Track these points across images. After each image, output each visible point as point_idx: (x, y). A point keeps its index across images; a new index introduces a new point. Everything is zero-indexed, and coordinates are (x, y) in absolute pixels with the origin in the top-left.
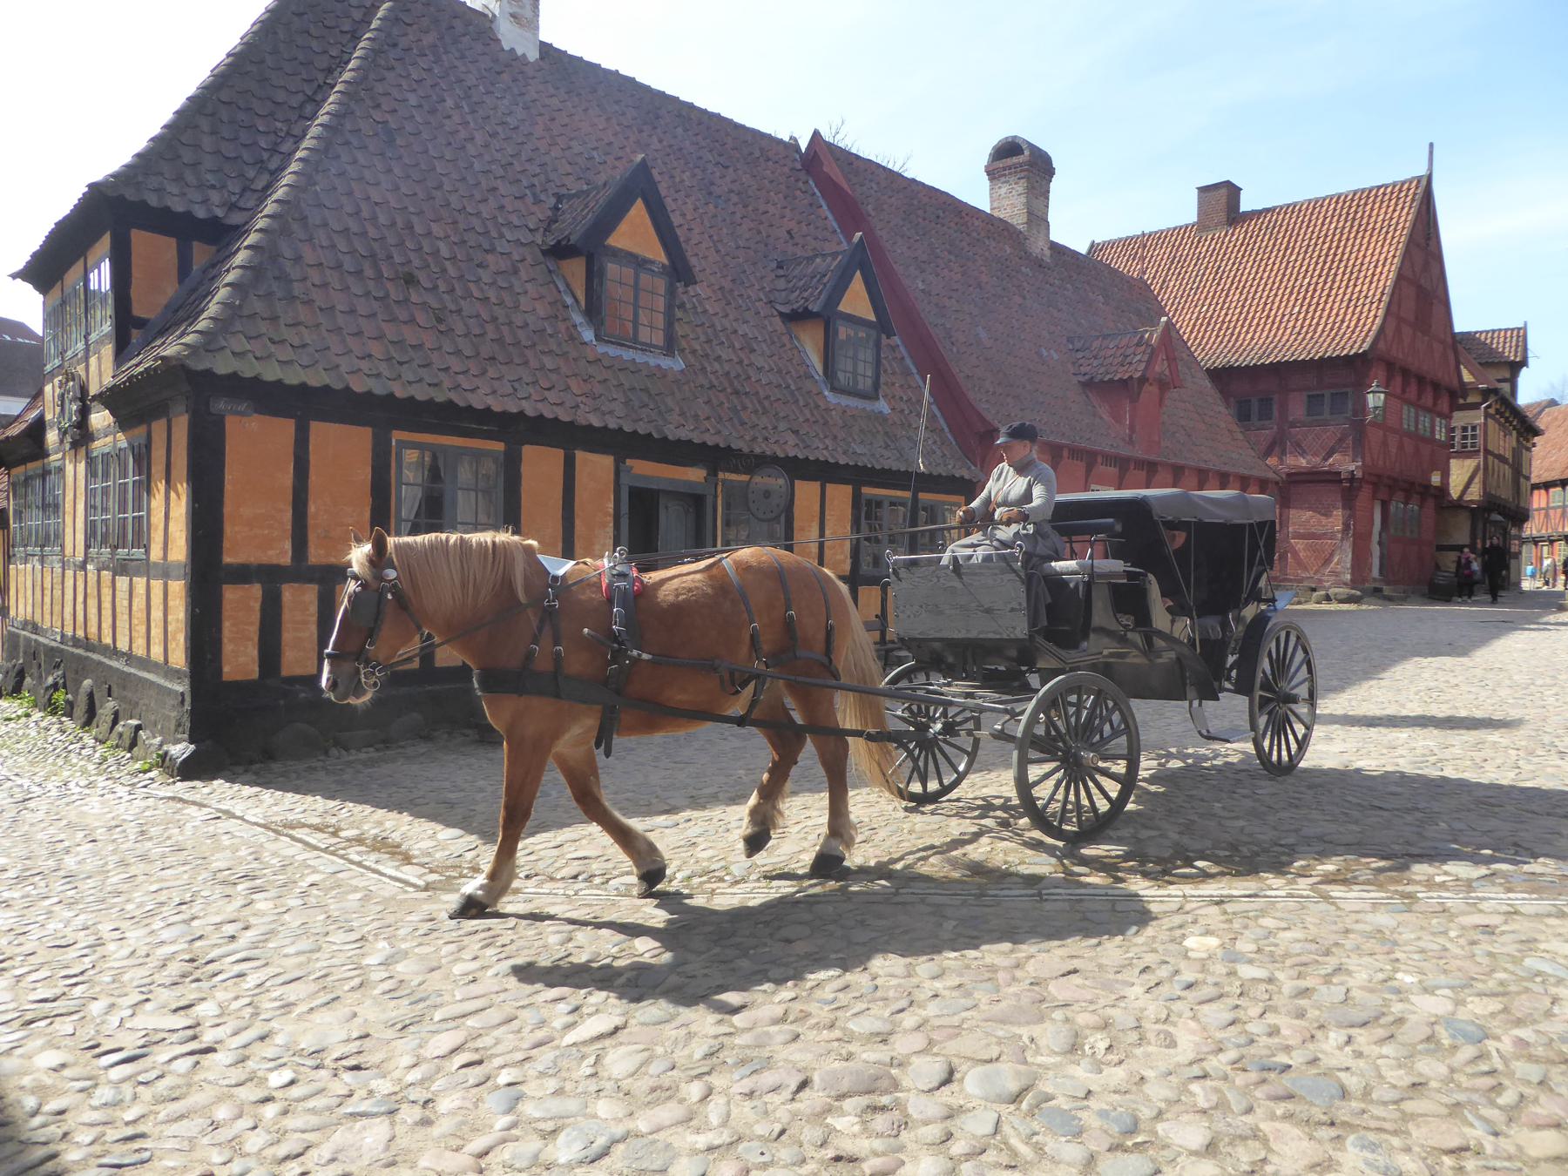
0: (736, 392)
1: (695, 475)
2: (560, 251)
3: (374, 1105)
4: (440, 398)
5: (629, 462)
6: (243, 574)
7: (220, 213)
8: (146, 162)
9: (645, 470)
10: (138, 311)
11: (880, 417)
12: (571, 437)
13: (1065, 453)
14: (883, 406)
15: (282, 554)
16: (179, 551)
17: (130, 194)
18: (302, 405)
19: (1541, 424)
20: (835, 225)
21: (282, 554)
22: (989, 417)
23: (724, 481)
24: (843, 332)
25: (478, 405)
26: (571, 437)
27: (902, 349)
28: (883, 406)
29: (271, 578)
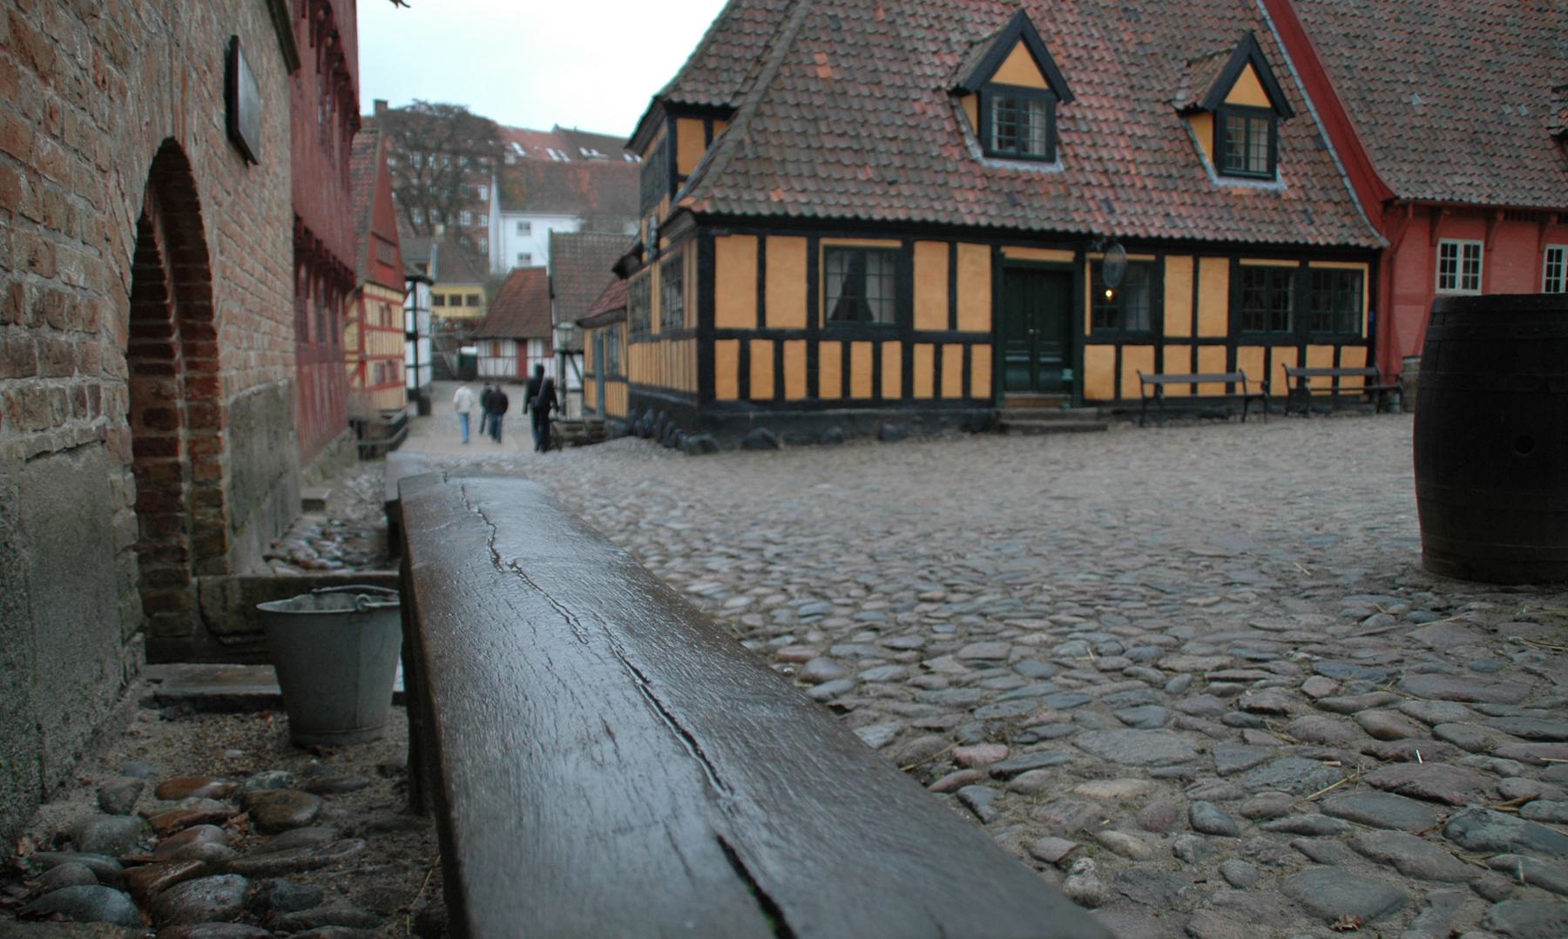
0: (1112, 186)
1: (1064, 256)
2: (959, 92)
3: (248, 100)
4: (849, 214)
5: (1003, 249)
6: (728, 334)
7: (728, 100)
8: (698, 64)
9: (1013, 253)
10: (682, 171)
11: (1277, 195)
12: (952, 234)
13: (1500, 217)
14: (1281, 184)
15: (751, 323)
16: (694, 323)
17: (676, 98)
18: (764, 227)
19: (613, 275)
20: (1265, 13)
21: (751, 323)
22: (1392, 186)
23: (1092, 261)
24: (1235, 125)
25: (877, 216)
26: (952, 234)
27: (1320, 126)
28: (1281, 184)
29: (743, 337)
